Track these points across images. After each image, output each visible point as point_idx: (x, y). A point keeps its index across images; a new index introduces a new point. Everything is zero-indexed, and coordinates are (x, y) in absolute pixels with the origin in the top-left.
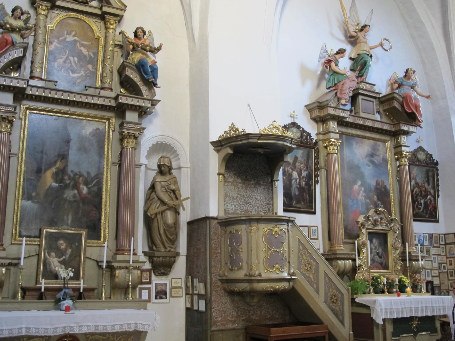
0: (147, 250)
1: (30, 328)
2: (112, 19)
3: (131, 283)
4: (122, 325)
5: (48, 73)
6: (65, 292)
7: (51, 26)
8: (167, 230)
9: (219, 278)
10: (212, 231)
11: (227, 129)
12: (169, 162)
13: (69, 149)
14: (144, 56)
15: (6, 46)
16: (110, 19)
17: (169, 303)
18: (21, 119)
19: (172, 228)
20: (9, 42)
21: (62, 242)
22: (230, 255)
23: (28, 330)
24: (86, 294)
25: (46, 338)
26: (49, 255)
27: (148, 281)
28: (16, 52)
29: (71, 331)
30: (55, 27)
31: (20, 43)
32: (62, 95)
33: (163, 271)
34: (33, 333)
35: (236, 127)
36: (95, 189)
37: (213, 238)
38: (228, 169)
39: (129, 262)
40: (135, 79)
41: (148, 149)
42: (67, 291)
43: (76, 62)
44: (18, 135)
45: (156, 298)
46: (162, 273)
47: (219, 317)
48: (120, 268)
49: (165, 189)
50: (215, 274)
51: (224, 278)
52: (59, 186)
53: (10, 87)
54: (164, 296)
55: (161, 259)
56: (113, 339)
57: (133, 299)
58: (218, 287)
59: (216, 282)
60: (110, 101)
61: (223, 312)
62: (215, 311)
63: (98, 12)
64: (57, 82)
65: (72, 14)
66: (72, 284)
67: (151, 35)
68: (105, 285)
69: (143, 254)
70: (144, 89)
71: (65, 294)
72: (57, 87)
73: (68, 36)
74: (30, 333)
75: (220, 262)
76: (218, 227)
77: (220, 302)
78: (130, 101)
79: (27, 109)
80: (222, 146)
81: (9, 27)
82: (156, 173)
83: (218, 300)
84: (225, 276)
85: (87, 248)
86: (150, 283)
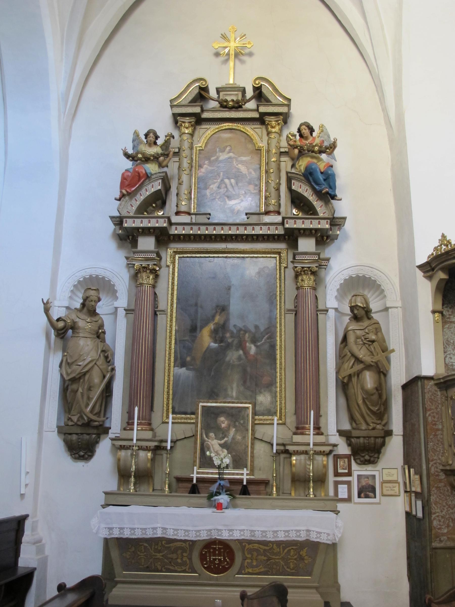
0: (347, 426)
1: (167, 529)
2: (272, 120)
3: (312, 475)
4: (288, 531)
5: (199, 205)
6: (220, 484)
7: (200, 145)
8: (367, 398)
9: (441, 467)
10: (426, 397)
11: (437, 244)
12: (363, 301)
13: (229, 298)
14: (315, 161)
15: (139, 180)
16: (270, 121)
17: (379, 503)
18: (168, 266)
19: (372, 395)
20: (141, 175)
21: (222, 419)
22: (453, 433)
23: (164, 531)
24: (200, 485)
25: (189, 543)
26: (207, 436)
27: (346, 471)
28: (153, 185)
29: (219, 535)
30: (204, 145)
31: (156, 174)
32: (215, 229)
33: (367, 457)
34: (170, 535)
35: (448, 239)
36: (266, 347)
37: (428, 408)
38: (450, 303)
39: (308, 444)
40: (306, 194)
41: (338, 287)
42: (222, 483)
43: (233, 184)
44: (166, 286)
45: (359, 497)
46: (366, 460)
47: (443, 527)
48: (297, 453)
49: (362, 340)
50: (434, 462)
51: (448, 468)
52: (219, 346)
53: (149, 228)
54: (371, 494)
55: (362, 440)
56: (278, 550)
57: (315, 496)
58: (440, 481)
59: (436, 473)
60: (277, 229)
61: (451, 520)
62: (437, 518)
63: (256, 115)
64: (210, 214)
65: (225, 125)
66: (212, 473)
67: (324, 130)
68: (276, 476)
69: (338, 434)
70: (318, 205)
71: (221, 487)
72: (210, 221)
73: (220, 154)
74: (167, 534)
75: (443, 444)
76: (436, 391)
77: (444, 504)
78: (299, 225)
79: (176, 253)
80: (433, 269)
81: (141, 156)
82: (350, 319)
83: (441, 502)
84: (449, 465)
85: (257, 427)
86: (349, 474)
